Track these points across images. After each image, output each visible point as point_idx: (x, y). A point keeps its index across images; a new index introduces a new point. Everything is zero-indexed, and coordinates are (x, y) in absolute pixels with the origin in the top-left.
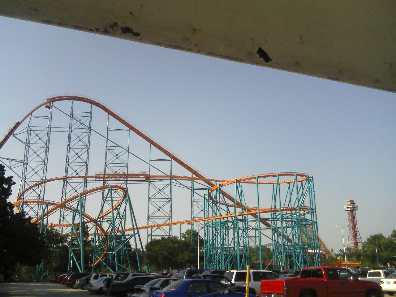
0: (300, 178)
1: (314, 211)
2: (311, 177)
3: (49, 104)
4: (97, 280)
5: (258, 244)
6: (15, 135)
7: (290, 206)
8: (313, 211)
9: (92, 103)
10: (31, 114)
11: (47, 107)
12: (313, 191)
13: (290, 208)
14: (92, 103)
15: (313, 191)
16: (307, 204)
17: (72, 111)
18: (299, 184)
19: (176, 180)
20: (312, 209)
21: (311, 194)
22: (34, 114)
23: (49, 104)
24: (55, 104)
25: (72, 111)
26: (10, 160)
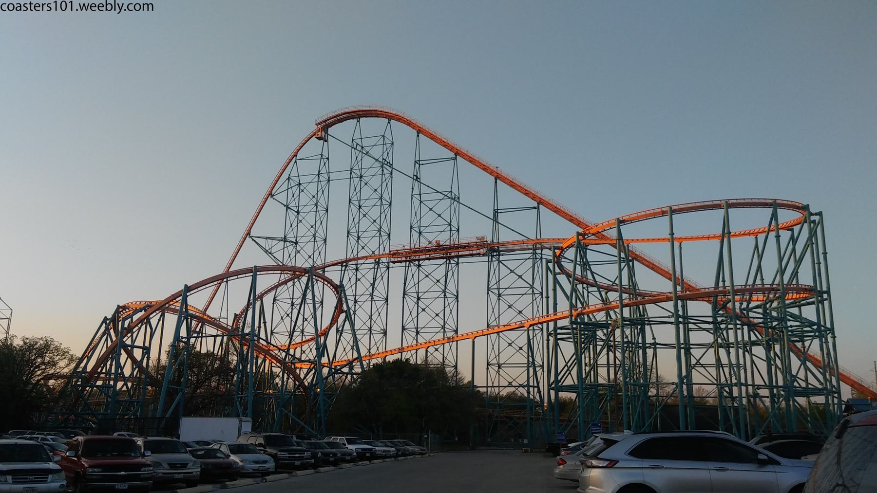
0: (786, 216)
1: (825, 296)
2: (816, 214)
3: (324, 129)
4: (823, 455)
5: (294, 265)
6: (273, 196)
7: (758, 282)
8: (822, 297)
9: (390, 117)
10: (296, 155)
11: (319, 138)
12: (821, 251)
13: (760, 286)
14: (390, 117)
15: (821, 251)
16: (806, 278)
17: (496, 208)
18: (785, 235)
19: (707, 331)
20: (821, 293)
21: (816, 261)
22: (299, 156)
23: (324, 129)
24: (331, 130)
25: (496, 208)
26: (267, 238)
